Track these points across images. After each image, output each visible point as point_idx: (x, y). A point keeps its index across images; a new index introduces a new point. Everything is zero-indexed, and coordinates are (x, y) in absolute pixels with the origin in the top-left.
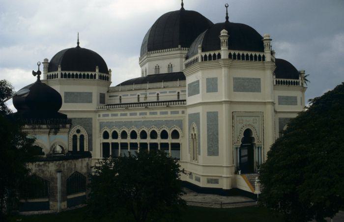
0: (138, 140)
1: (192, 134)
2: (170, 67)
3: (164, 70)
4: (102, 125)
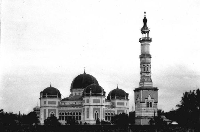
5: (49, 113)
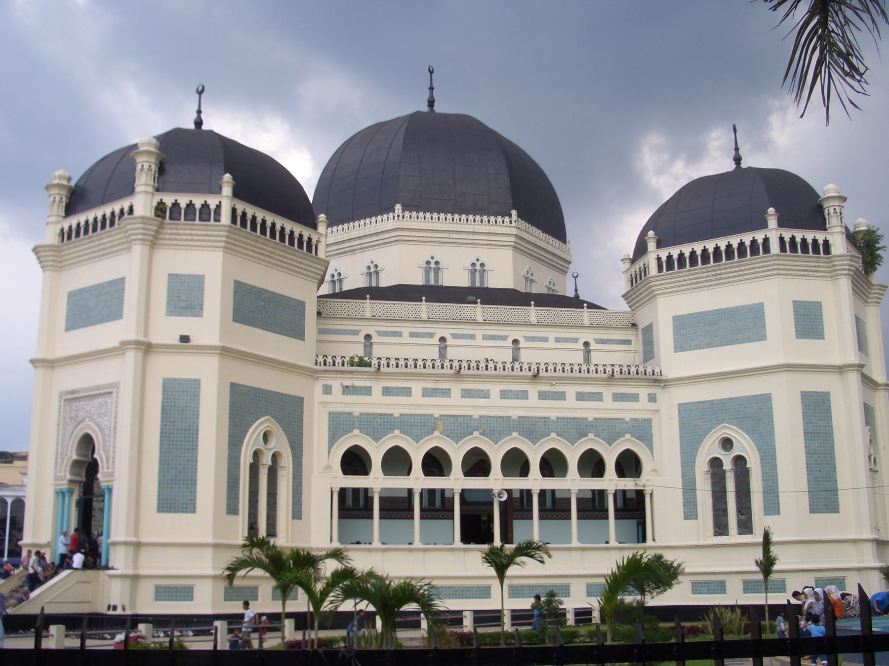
0: (456, 482)
1: (716, 463)
2: (478, 269)
3: (455, 276)
4: (339, 424)
5: (235, 442)
